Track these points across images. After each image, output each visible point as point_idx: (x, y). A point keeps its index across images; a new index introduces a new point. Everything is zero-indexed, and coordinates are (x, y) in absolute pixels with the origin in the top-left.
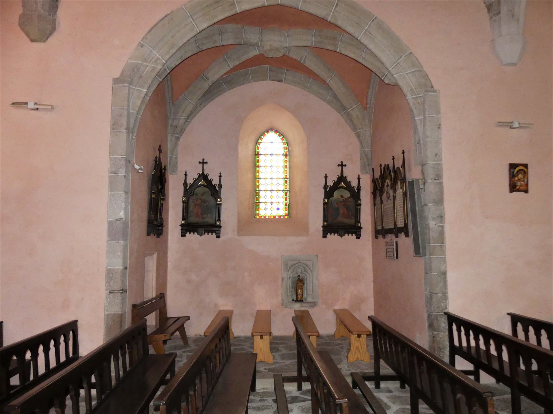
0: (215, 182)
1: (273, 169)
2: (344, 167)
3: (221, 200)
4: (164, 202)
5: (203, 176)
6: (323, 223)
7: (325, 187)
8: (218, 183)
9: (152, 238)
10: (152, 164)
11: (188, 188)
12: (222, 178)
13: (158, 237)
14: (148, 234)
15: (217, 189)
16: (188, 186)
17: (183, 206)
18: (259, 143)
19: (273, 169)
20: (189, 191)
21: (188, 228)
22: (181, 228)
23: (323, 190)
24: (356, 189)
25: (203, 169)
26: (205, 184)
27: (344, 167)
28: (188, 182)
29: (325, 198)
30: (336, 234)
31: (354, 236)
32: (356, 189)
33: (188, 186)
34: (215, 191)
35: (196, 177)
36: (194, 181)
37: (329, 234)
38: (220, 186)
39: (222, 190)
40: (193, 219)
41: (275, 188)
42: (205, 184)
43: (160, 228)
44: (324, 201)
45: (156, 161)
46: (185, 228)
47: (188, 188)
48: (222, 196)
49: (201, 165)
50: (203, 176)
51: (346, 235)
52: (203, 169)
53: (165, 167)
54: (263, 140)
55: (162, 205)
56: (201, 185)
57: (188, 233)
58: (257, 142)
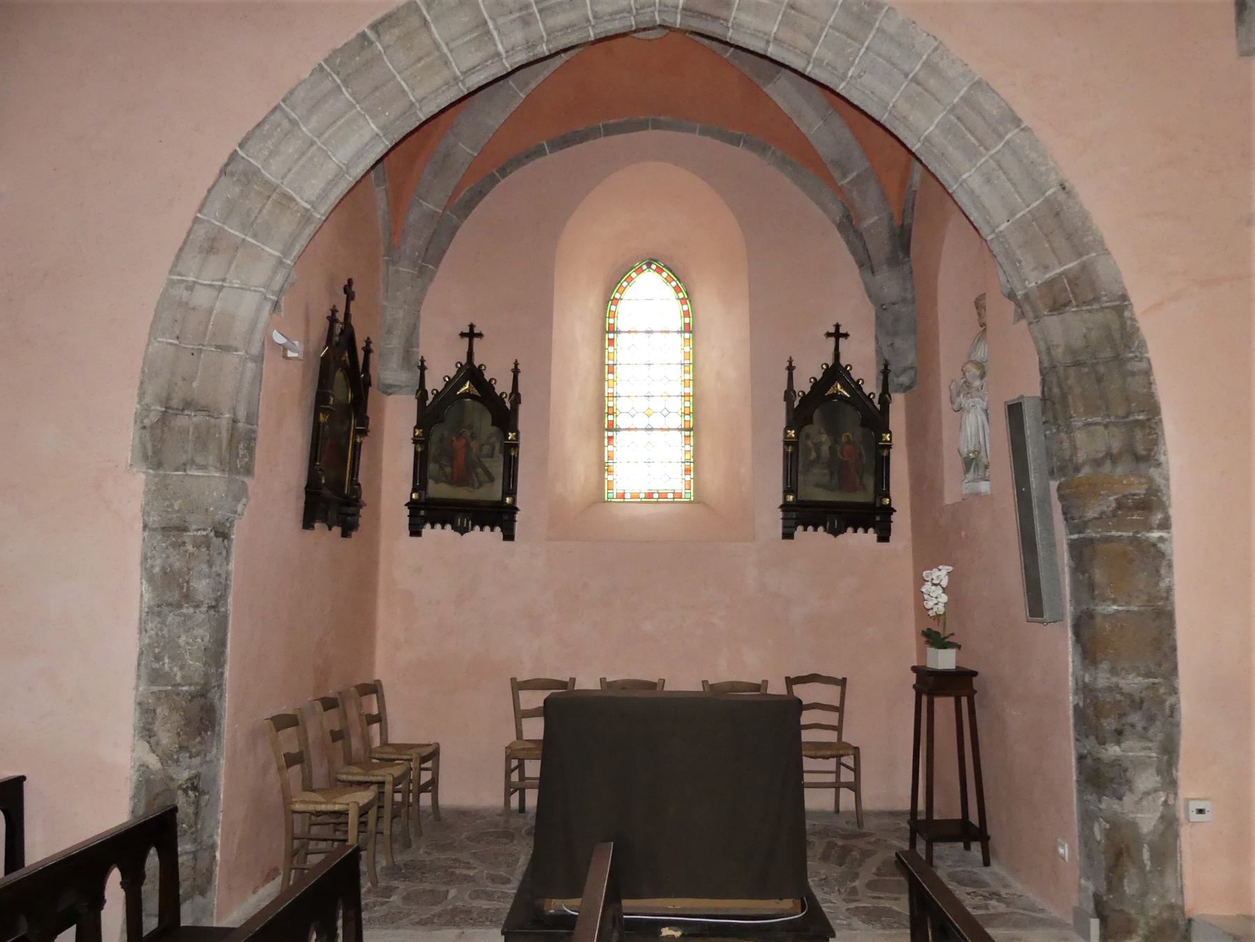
0: (503, 387)
1: (650, 386)
2: (842, 340)
3: (517, 437)
4: (365, 440)
5: (471, 371)
6: (785, 498)
7: (789, 394)
8: (509, 391)
9: (325, 537)
10: (319, 328)
11: (428, 403)
12: (520, 377)
13: (345, 534)
14: (308, 524)
15: (508, 405)
16: (431, 397)
17: (416, 453)
18: (616, 301)
19: (650, 386)
20: (433, 414)
21: (424, 513)
22: (780, 515)
23: (783, 405)
24: (876, 401)
25: (470, 354)
26: (476, 392)
27: (842, 340)
28: (429, 387)
29: (788, 427)
30: (821, 529)
31: (872, 535)
32: (876, 401)
33: (431, 397)
34: (504, 415)
35: (452, 372)
36: (447, 384)
37: (800, 528)
38: (516, 396)
39: (522, 409)
40: (438, 490)
41: (657, 421)
42: (476, 392)
43: (351, 510)
44: (786, 433)
45: (332, 320)
46: (794, 515)
47: (428, 403)
48: (520, 427)
49: (467, 340)
50: (471, 371)
51: (850, 530)
52: (470, 354)
53: (368, 342)
54: (626, 295)
55: (357, 448)
56: (466, 395)
57: (428, 526)
58: (608, 299)
